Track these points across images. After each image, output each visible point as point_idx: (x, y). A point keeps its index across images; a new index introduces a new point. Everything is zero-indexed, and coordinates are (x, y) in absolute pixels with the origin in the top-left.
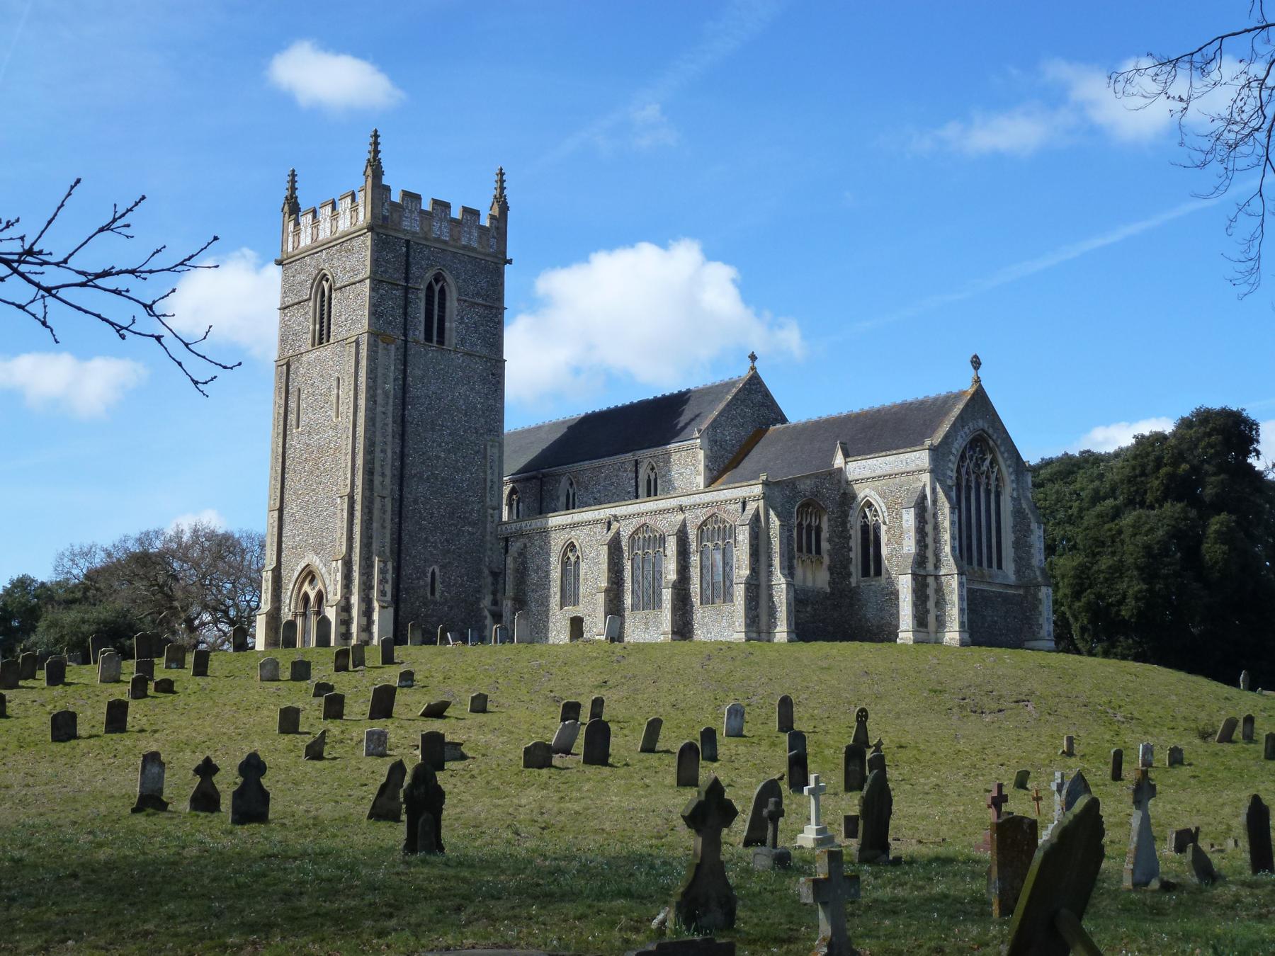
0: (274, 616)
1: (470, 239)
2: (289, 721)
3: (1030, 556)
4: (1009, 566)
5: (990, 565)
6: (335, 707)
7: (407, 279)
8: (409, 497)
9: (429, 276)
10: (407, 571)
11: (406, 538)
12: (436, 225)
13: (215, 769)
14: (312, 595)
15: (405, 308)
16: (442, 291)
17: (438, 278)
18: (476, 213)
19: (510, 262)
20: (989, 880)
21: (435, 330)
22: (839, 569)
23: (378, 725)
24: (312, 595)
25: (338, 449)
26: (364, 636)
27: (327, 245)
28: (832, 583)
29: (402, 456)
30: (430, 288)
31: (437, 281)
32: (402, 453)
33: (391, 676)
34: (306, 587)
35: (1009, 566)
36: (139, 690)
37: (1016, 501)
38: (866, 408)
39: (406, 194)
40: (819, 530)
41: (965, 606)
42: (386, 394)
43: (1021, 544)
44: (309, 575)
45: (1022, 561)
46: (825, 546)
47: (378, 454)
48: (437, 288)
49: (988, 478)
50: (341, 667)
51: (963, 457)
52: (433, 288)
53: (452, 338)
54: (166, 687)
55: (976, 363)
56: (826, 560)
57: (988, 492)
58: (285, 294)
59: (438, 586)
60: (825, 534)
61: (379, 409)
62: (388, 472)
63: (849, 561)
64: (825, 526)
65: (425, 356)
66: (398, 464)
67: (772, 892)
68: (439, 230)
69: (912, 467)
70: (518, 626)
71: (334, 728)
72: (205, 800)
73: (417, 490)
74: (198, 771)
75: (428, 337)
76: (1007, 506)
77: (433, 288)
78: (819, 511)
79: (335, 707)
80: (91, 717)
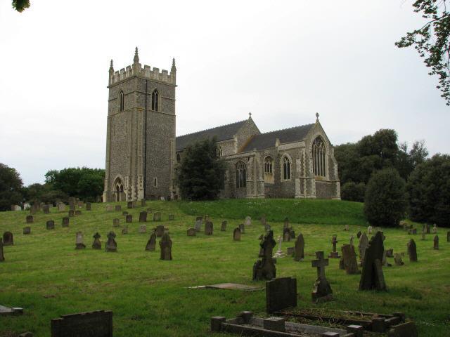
0: (108, 192)
1: (165, 79)
2: (116, 221)
3: (334, 172)
6: (129, 218)
8: (148, 156)
9: (153, 90)
10: (148, 179)
11: (147, 169)
12: (155, 75)
13: (99, 236)
14: (120, 186)
17: (156, 91)
18: (167, 72)
19: (141, 95)
21: (155, 106)
22: (277, 177)
23: (29, 225)
24: (120, 186)
25: (127, 142)
26: (135, 198)
27: (123, 82)
28: (275, 181)
30: (153, 94)
32: (146, 144)
33: (145, 209)
35: (328, 176)
36: (71, 212)
37: (330, 156)
38: (285, 129)
39: (145, 66)
40: (271, 165)
42: (141, 126)
43: (331, 169)
44: (119, 180)
45: (332, 174)
46: (273, 170)
47: (139, 144)
50: (129, 208)
51: (314, 143)
53: (160, 109)
54: (79, 212)
55: (317, 115)
56: (274, 174)
57: (321, 154)
58: (110, 96)
59: (157, 183)
60: (273, 167)
61: (139, 131)
62: (141, 149)
64: (273, 164)
65: (151, 115)
67: (127, 267)
68: (156, 77)
69: (299, 146)
70: (99, 200)
71: (130, 225)
72: (97, 246)
73: (150, 154)
74: (94, 237)
75: (153, 109)
76: (327, 158)
78: (272, 160)
79: (129, 218)
80: (58, 222)
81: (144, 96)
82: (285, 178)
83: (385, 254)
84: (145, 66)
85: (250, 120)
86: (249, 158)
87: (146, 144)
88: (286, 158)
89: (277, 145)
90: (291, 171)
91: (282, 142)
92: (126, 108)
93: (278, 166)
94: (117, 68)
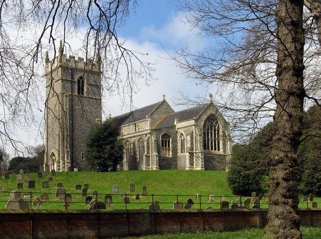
4: (221, 150)
5: (212, 149)
7: (72, 79)
15: (72, 86)
16: (83, 82)
18: (83, 59)
20: (244, 208)
29: (72, 124)
30: (79, 81)
31: (81, 79)
34: (53, 157)
35: (221, 150)
40: (169, 142)
41: (203, 164)
48: (81, 81)
49: (215, 126)
51: (206, 121)
52: (79, 82)
55: (164, 96)
57: (215, 131)
60: (171, 143)
63: (172, 151)
66: (71, 126)
73: (77, 132)
77: (79, 82)
81: (271, 97)
82: (182, 153)
83: (225, 209)
84: (70, 57)
85: (164, 101)
86: (146, 135)
87: (72, 124)
88: (182, 134)
89: (175, 123)
90: (185, 146)
91: (180, 120)
92: (153, 116)
93: (175, 142)
94: (68, 53)
